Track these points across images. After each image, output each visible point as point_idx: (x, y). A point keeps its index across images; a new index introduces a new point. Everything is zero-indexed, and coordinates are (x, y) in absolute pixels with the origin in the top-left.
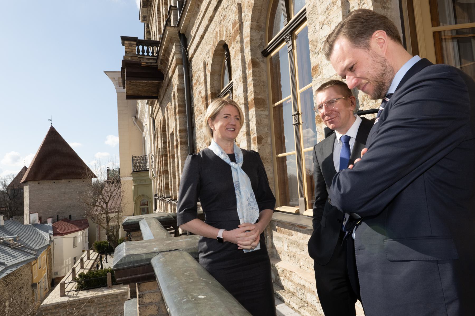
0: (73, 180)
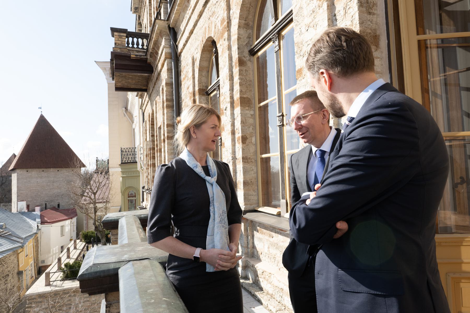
0: (62, 169)
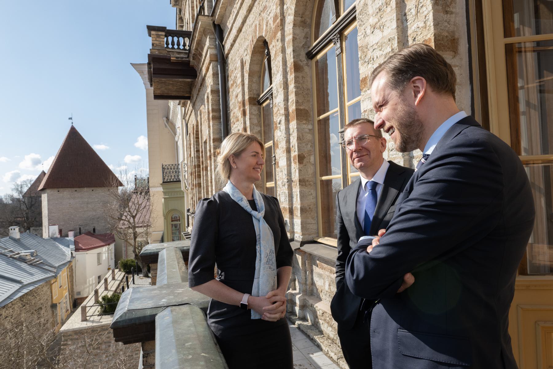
0: (97, 188)
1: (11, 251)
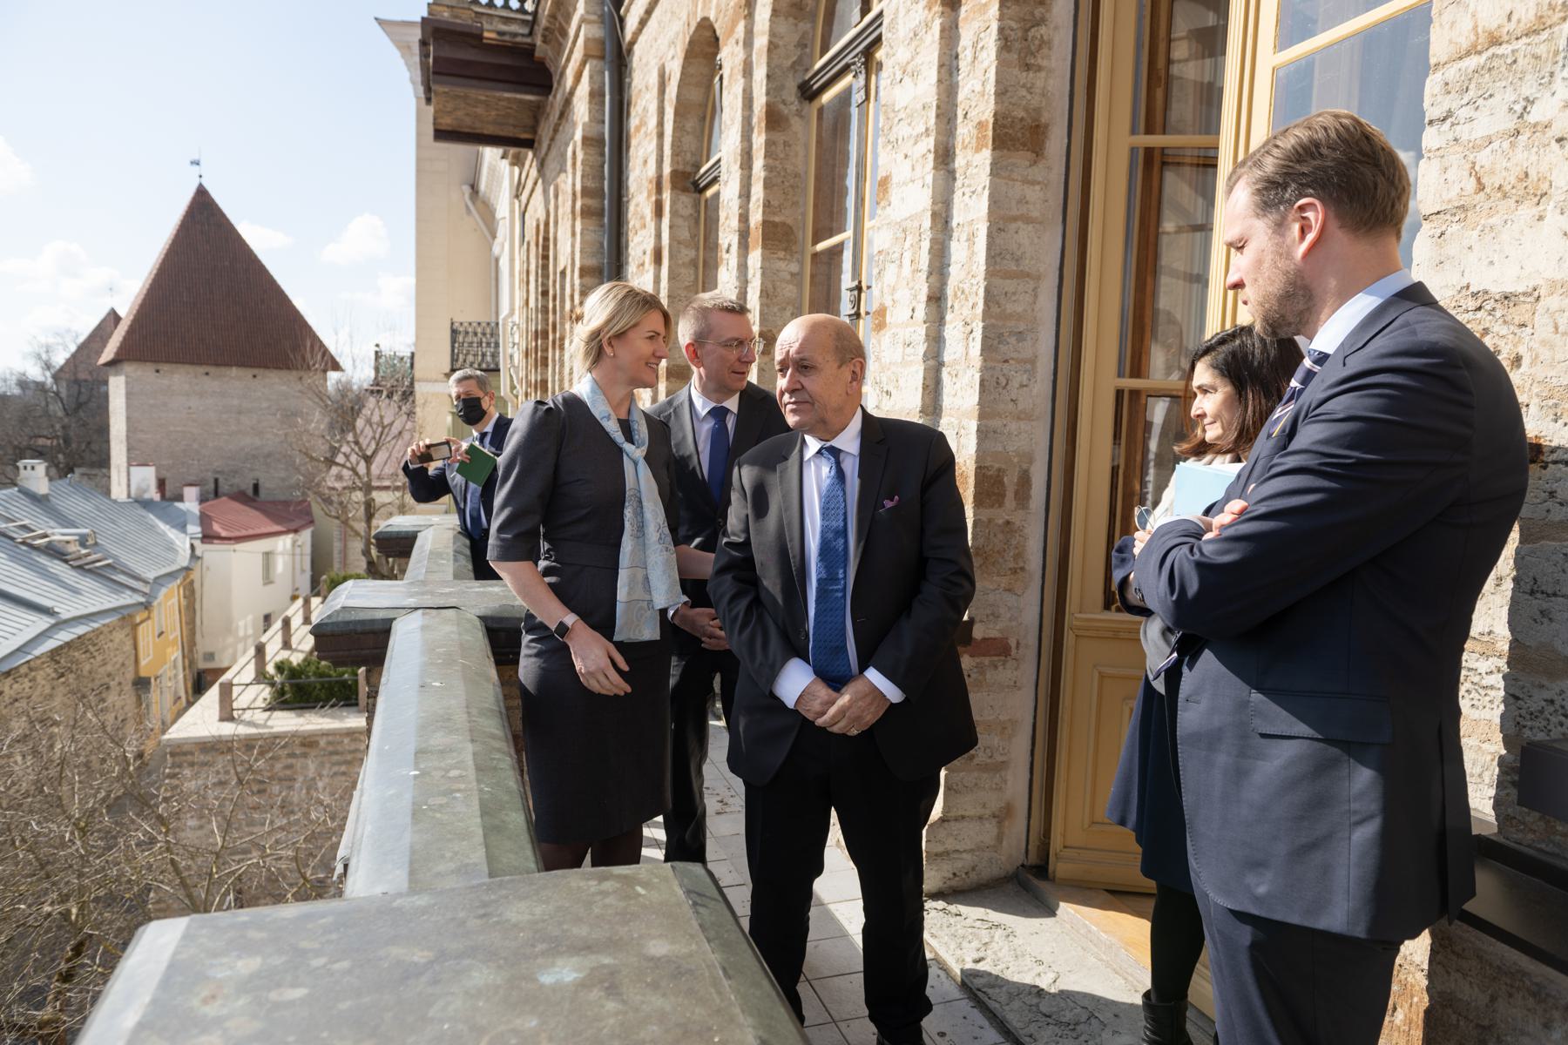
0: (267, 372)
1: (24, 527)
